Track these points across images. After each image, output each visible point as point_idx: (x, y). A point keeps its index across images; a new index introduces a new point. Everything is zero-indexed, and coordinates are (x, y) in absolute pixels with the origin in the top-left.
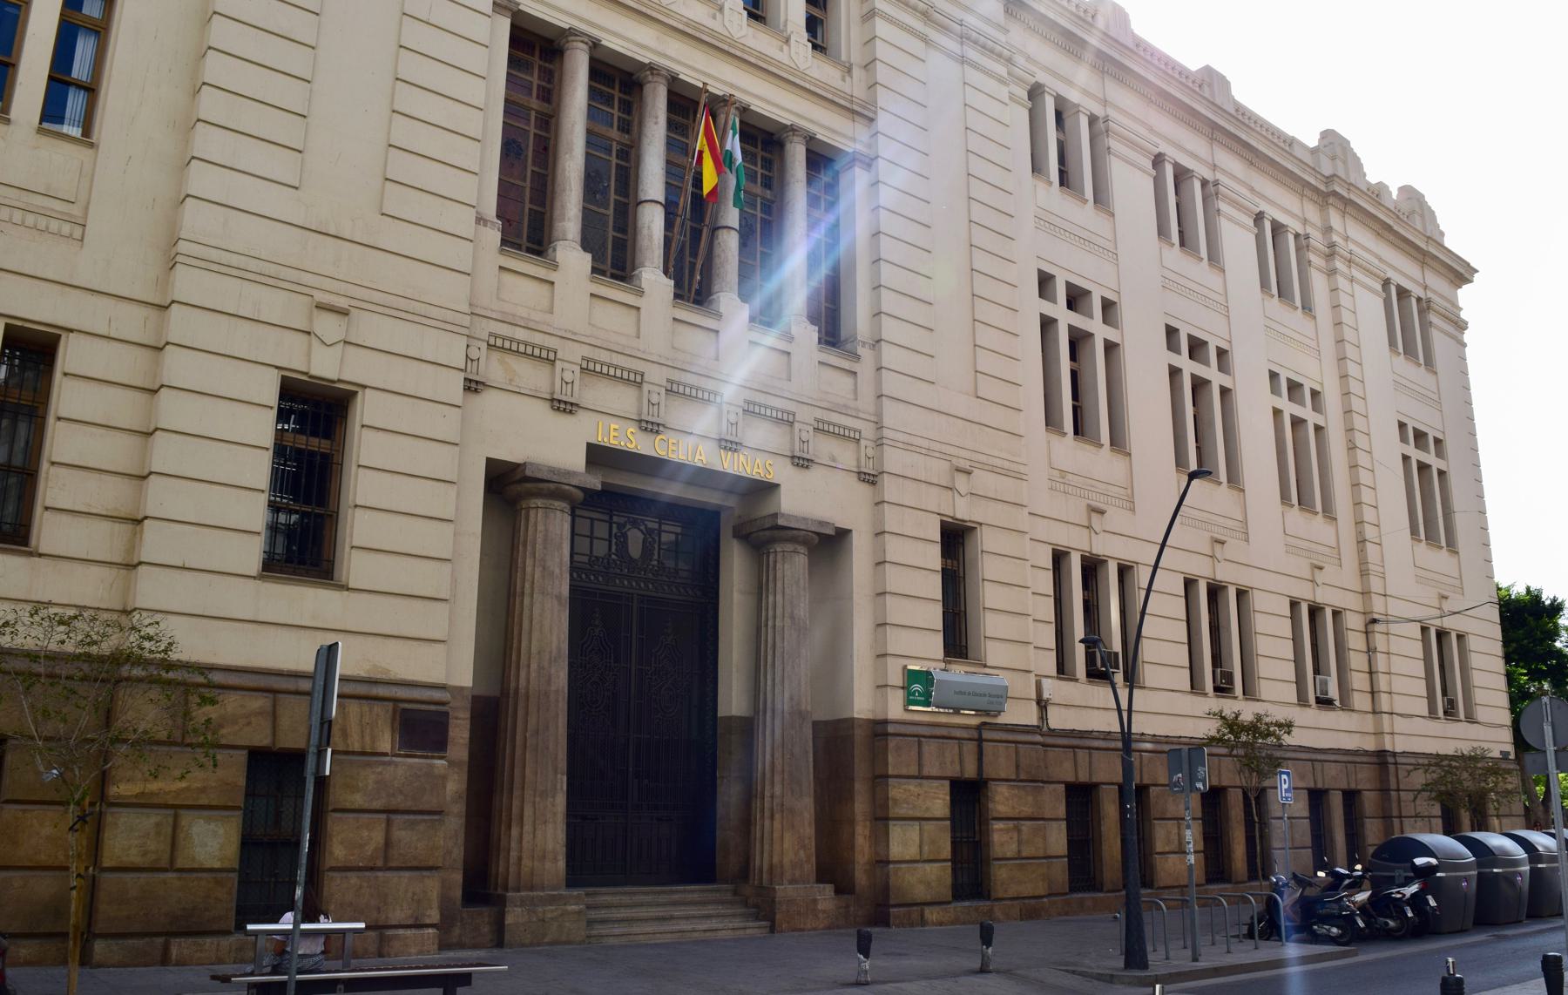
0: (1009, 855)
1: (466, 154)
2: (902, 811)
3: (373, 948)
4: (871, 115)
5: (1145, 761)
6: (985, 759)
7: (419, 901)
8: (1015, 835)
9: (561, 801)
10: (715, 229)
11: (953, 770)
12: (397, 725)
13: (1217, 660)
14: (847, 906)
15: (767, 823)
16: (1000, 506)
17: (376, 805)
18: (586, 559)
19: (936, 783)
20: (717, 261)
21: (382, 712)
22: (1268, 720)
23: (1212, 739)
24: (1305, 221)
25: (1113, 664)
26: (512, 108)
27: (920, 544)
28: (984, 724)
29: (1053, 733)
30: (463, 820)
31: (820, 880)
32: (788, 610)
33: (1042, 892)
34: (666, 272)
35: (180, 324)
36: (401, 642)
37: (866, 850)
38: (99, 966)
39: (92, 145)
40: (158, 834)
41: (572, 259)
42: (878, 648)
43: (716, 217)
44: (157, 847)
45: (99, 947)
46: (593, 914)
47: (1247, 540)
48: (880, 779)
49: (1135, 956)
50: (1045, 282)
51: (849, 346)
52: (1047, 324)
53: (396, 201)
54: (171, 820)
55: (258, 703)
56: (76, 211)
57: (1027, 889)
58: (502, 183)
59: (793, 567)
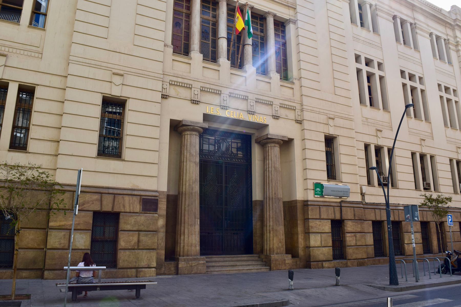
0: (352, 245)
1: (161, 26)
2: (314, 230)
3: (134, 274)
4: (295, 7)
5: (400, 213)
6: (343, 213)
7: (149, 260)
8: (355, 238)
9: (197, 228)
10: (244, 45)
11: (332, 217)
12: (141, 203)
13: (424, 179)
14: (296, 262)
15: (268, 234)
16: (345, 129)
17: (135, 229)
18: (207, 151)
19: (326, 221)
20: (245, 55)
21: (136, 199)
22: (442, 197)
23: (423, 204)
24: (447, 35)
25: (387, 181)
26: (176, 12)
27: (318, 143)
28: (342, 201)
29: (367, 204)
30: (164, 234)
31: (287, 253)
32: (273, 165)
33: (365, 257)
34: (228, 59)
35: (71, 81)
36: (142, 177)
37: (303, 243)
38: (46, 279)
39: (44, 30)
40: (64, 238)
41: (196, 55)
42: (305, 177)
43: (244, 41)
44: (64, 242)
45: (46, 273)
46: (210, 264)
47: (433, 139)
48: (306, 220)
49: (393, 280)
50: (357, 58)
51: (291, 80)
52: (359, 71)
53: (138, 40)
54: (68, 233)
55: (96, 197)
56: (39, 50)
57: (359, 256)
58: (173, 35)
59: (274, 151)
